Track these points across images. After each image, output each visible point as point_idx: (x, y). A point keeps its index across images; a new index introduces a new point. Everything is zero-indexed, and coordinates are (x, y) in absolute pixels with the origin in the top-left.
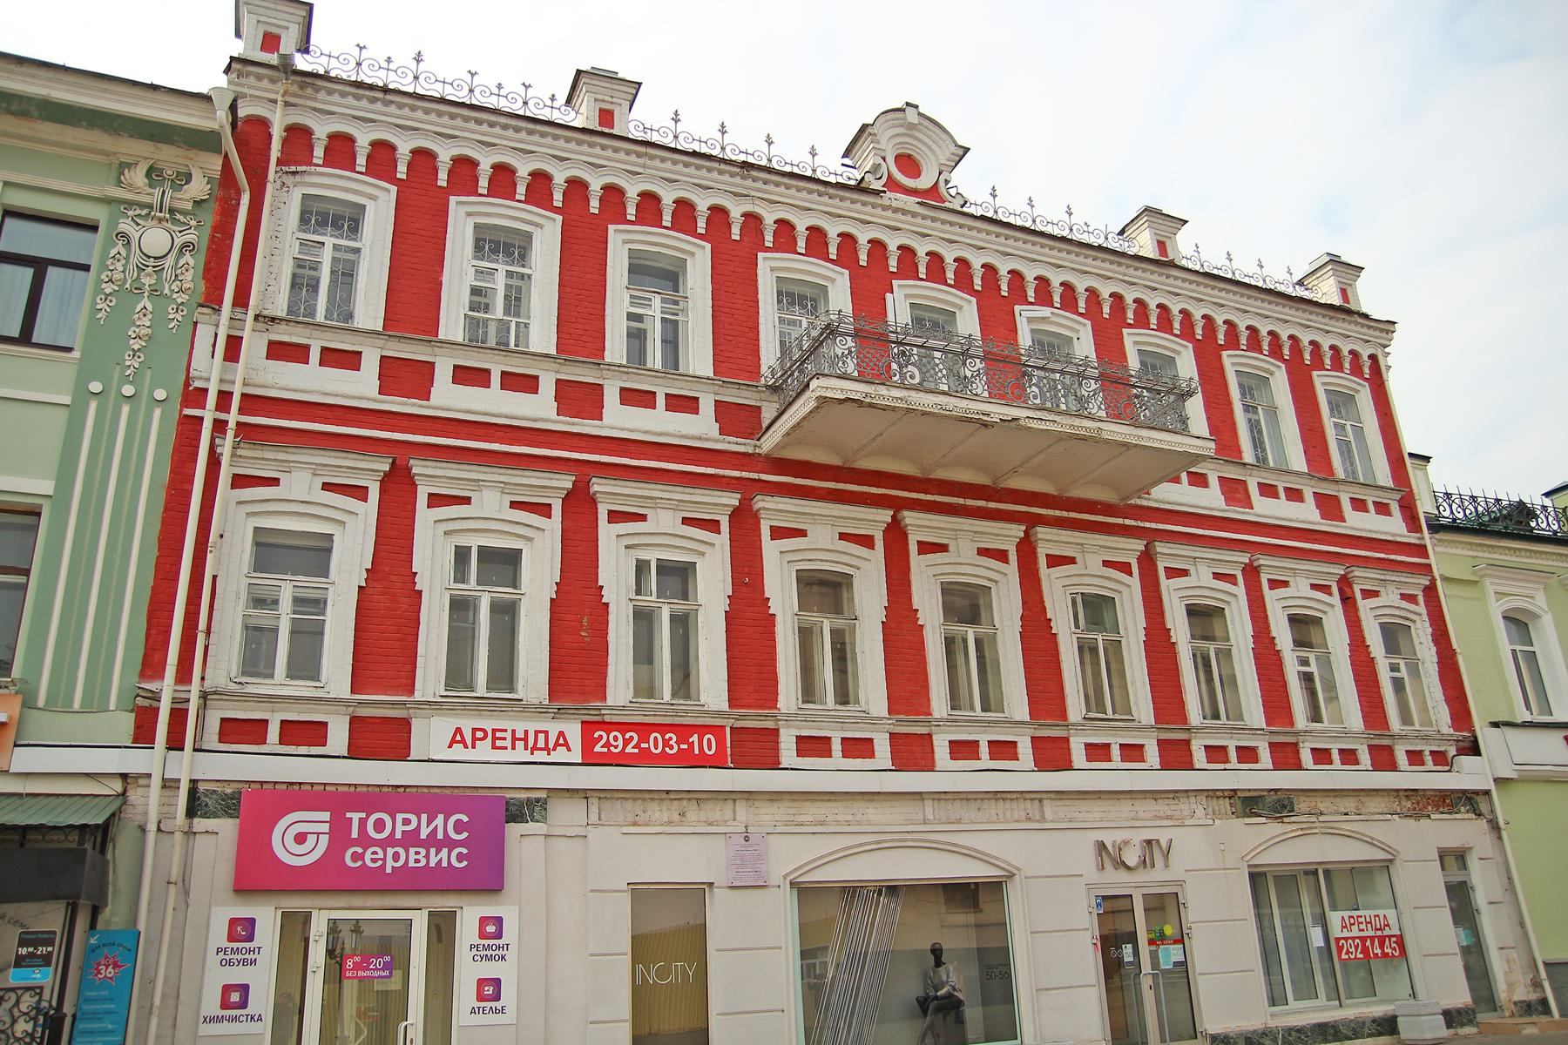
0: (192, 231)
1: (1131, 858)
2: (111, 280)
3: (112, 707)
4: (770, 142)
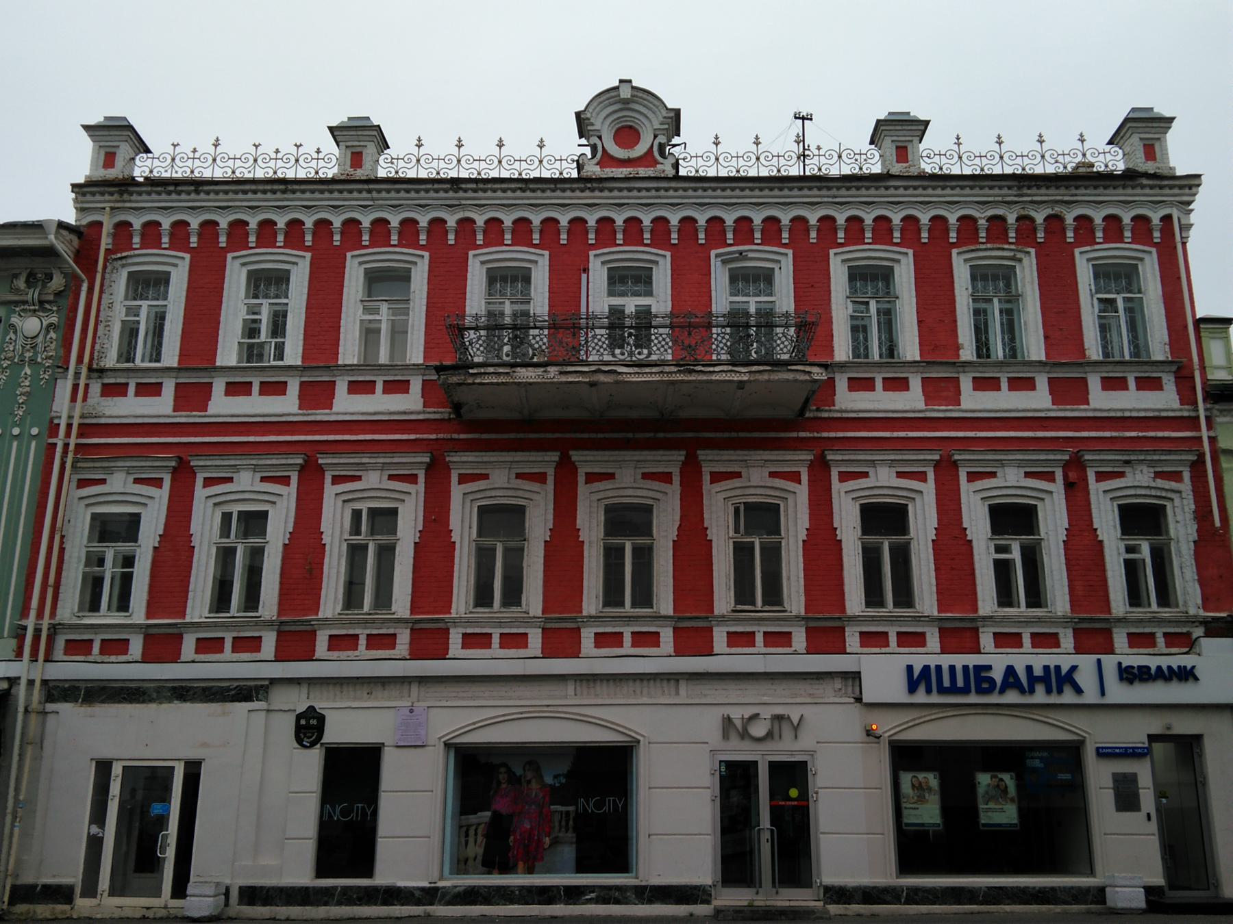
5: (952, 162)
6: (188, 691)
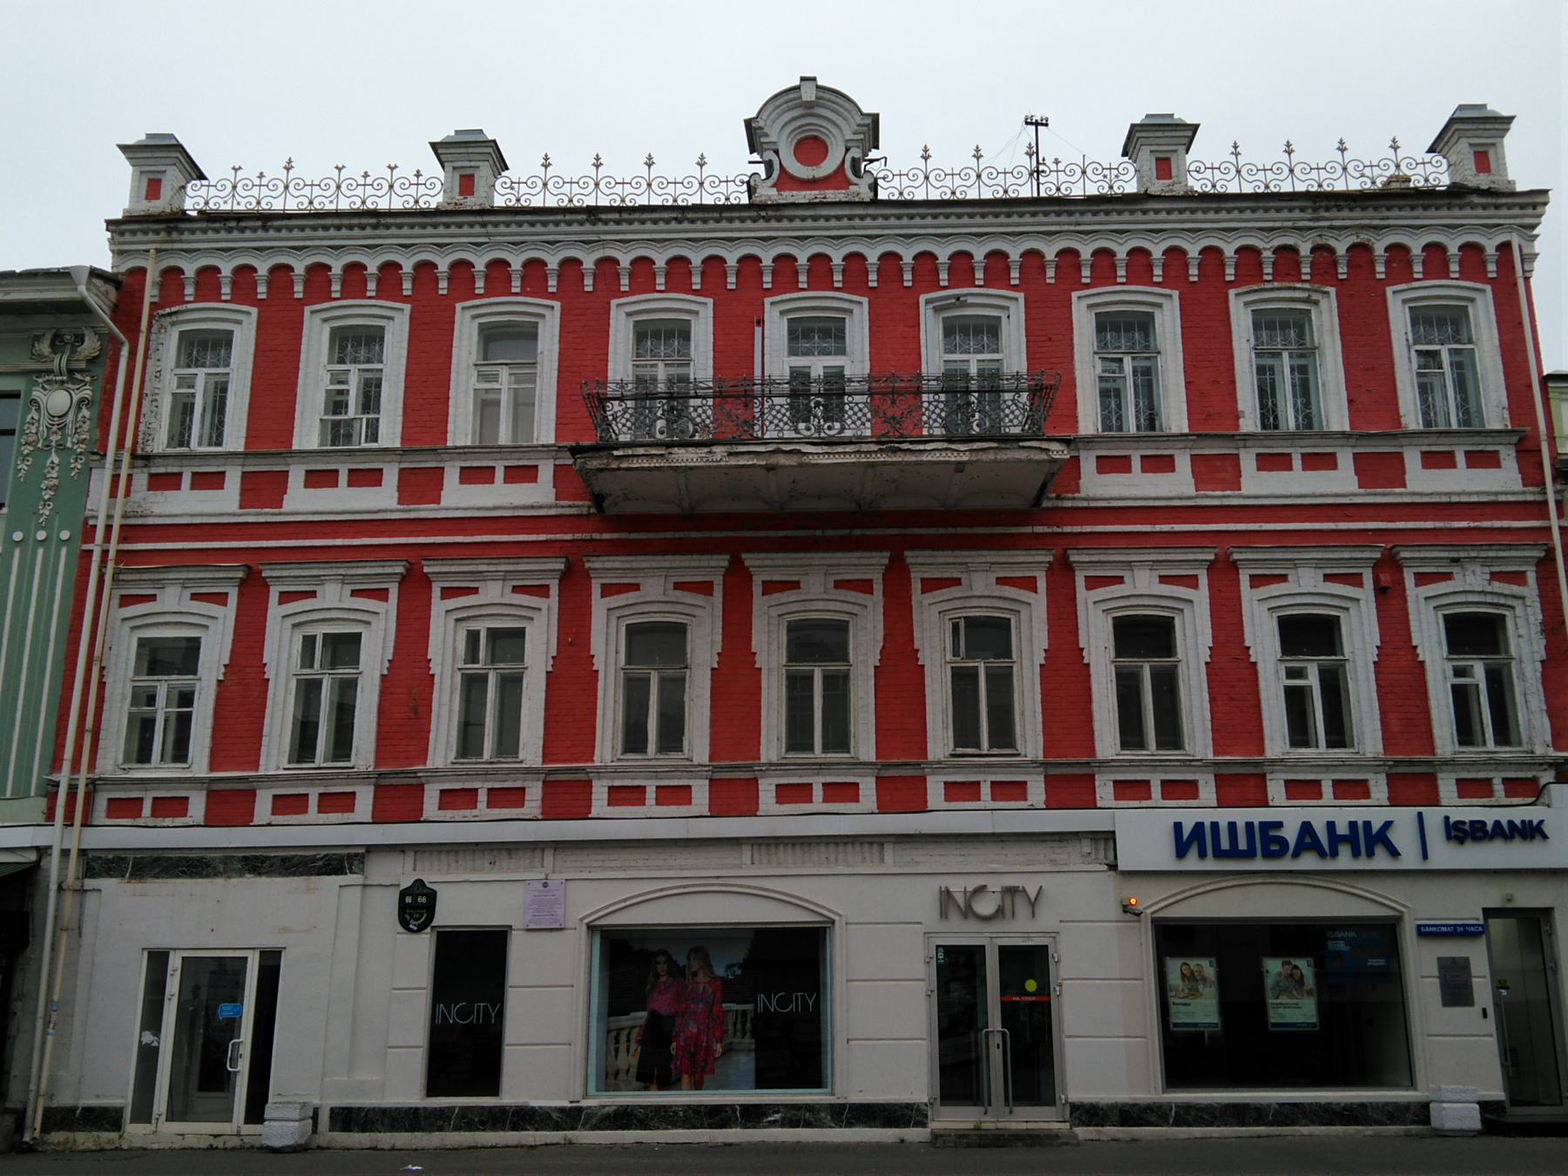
0: (87, 387)
2: (26, 443)
3: (32, 794)
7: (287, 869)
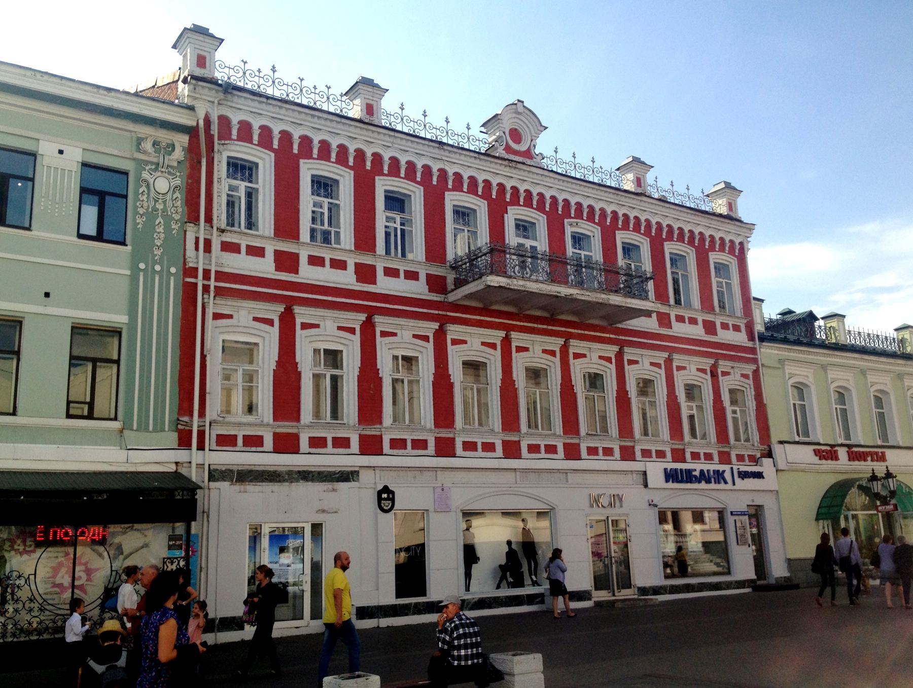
0: (177, 179)
1: (604, 501)
4: (447, 122)
5: (268, 84)
6: (308, 474)
7: (321, 478)
